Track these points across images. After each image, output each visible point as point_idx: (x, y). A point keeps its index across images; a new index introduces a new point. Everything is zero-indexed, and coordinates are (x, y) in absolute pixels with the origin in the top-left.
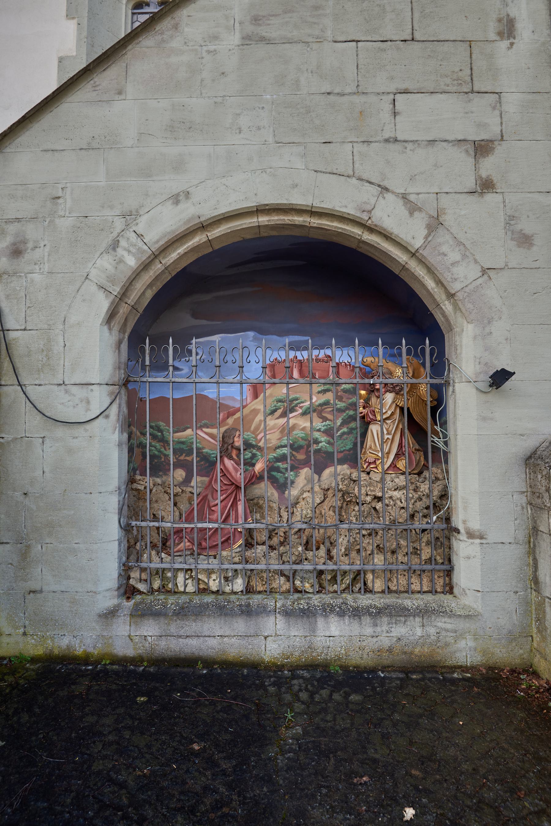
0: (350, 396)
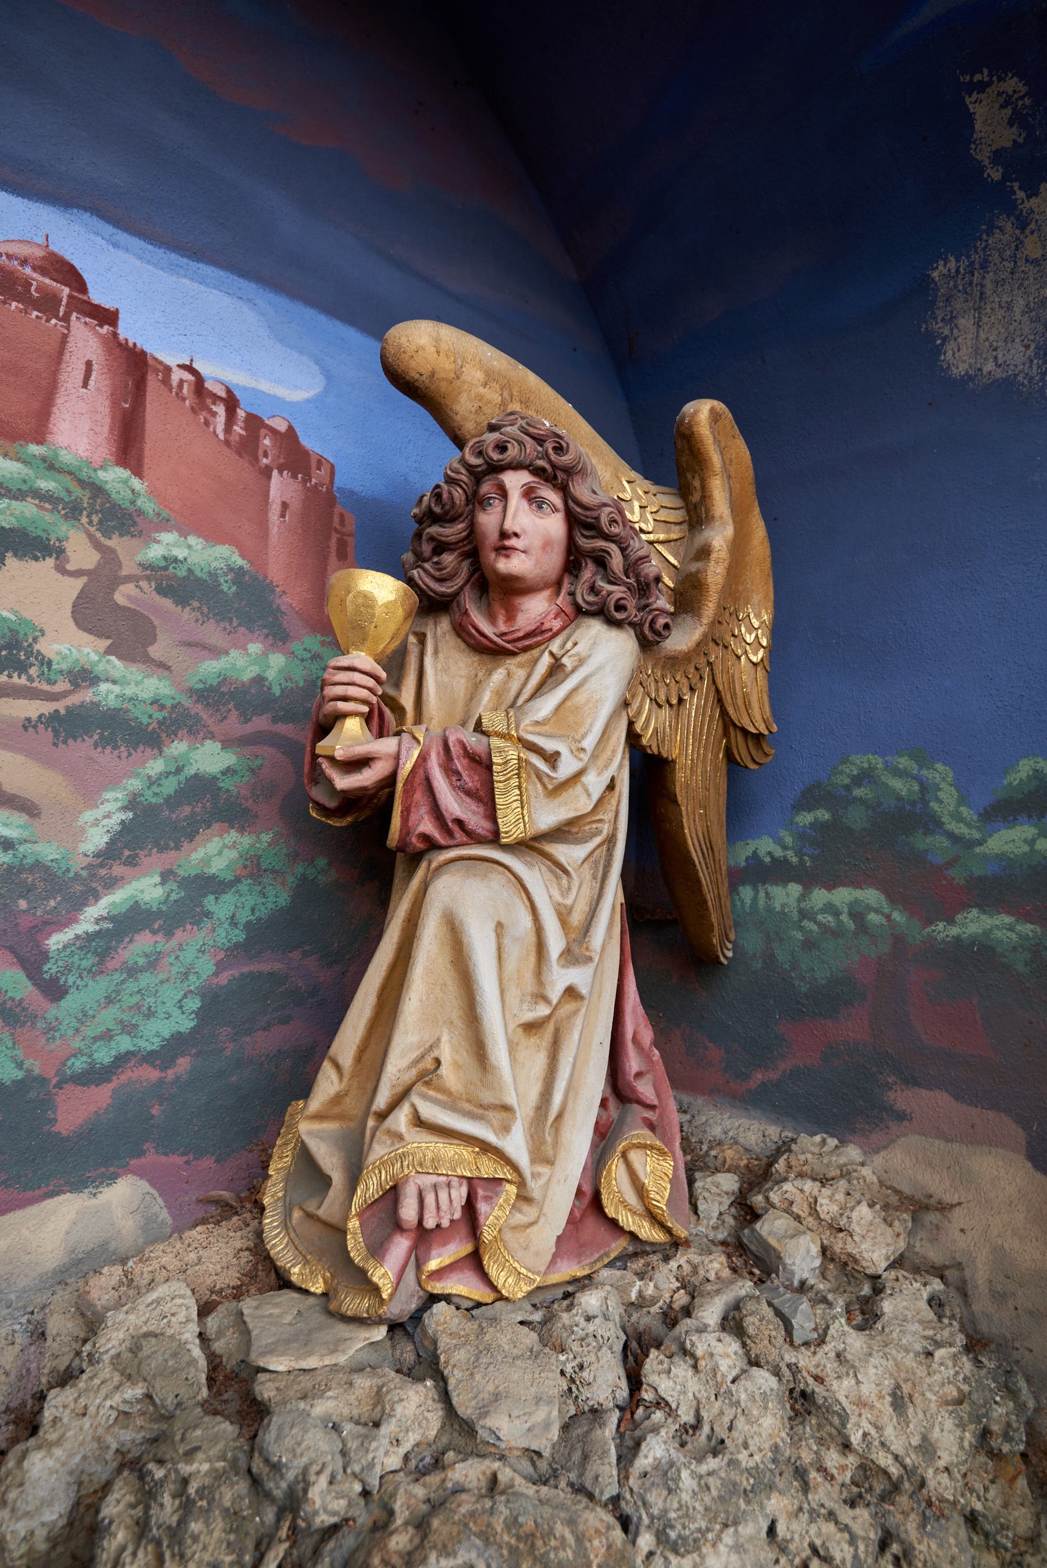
0: (212, 633)
